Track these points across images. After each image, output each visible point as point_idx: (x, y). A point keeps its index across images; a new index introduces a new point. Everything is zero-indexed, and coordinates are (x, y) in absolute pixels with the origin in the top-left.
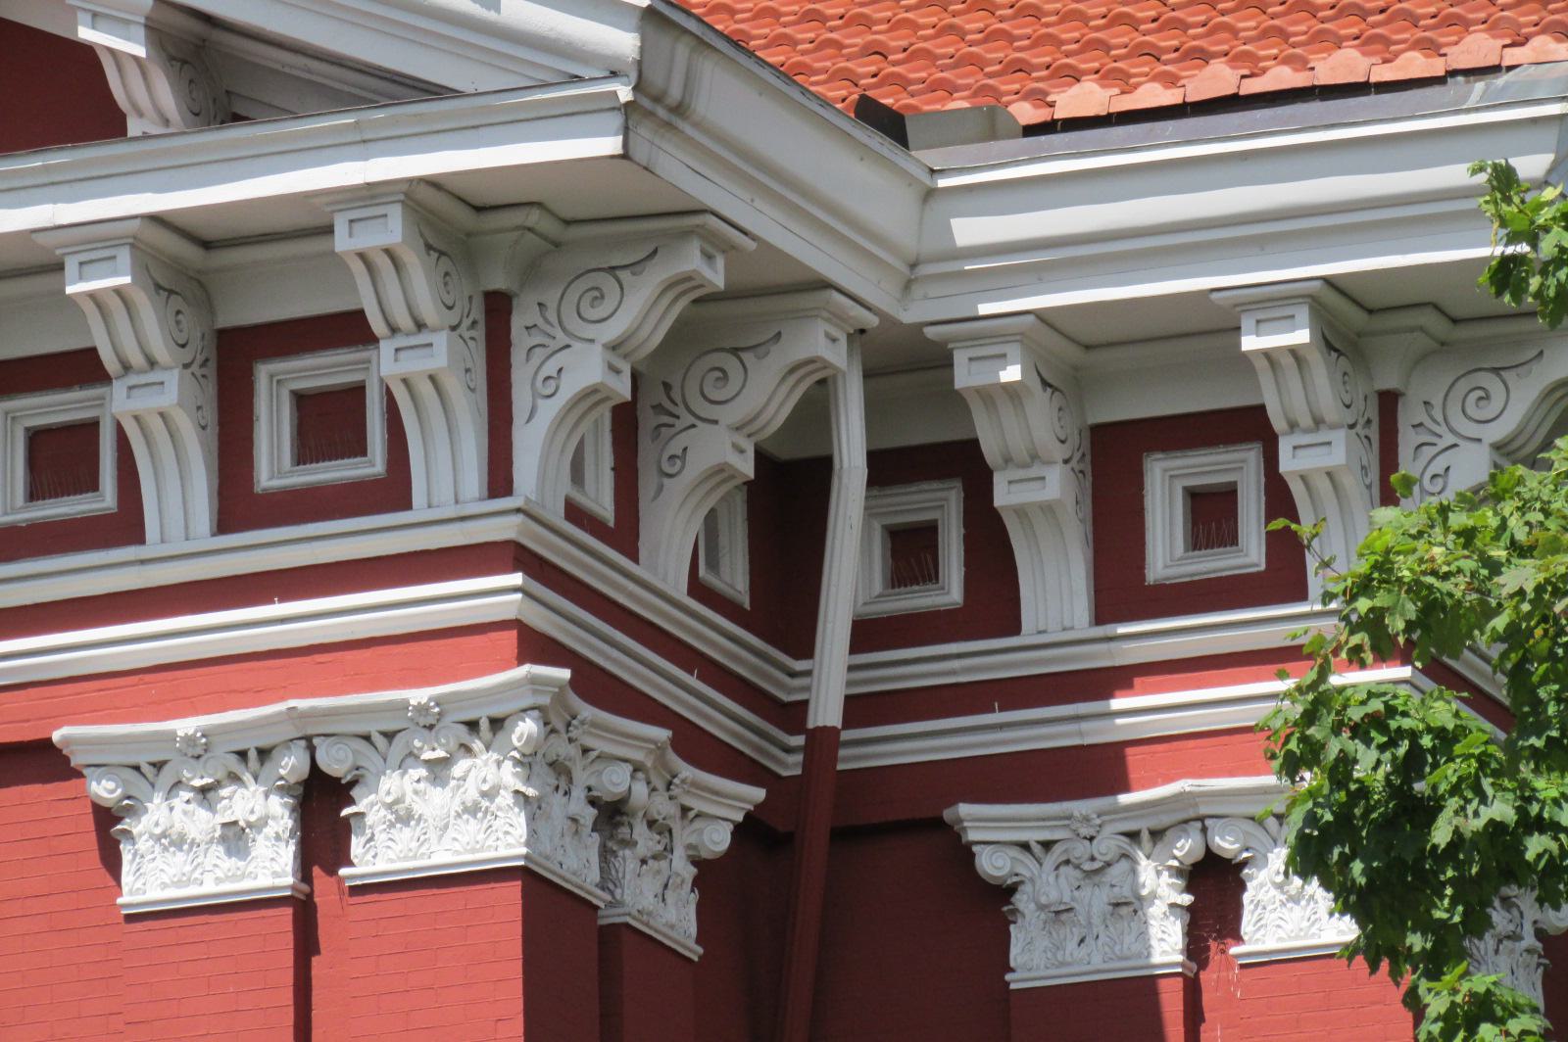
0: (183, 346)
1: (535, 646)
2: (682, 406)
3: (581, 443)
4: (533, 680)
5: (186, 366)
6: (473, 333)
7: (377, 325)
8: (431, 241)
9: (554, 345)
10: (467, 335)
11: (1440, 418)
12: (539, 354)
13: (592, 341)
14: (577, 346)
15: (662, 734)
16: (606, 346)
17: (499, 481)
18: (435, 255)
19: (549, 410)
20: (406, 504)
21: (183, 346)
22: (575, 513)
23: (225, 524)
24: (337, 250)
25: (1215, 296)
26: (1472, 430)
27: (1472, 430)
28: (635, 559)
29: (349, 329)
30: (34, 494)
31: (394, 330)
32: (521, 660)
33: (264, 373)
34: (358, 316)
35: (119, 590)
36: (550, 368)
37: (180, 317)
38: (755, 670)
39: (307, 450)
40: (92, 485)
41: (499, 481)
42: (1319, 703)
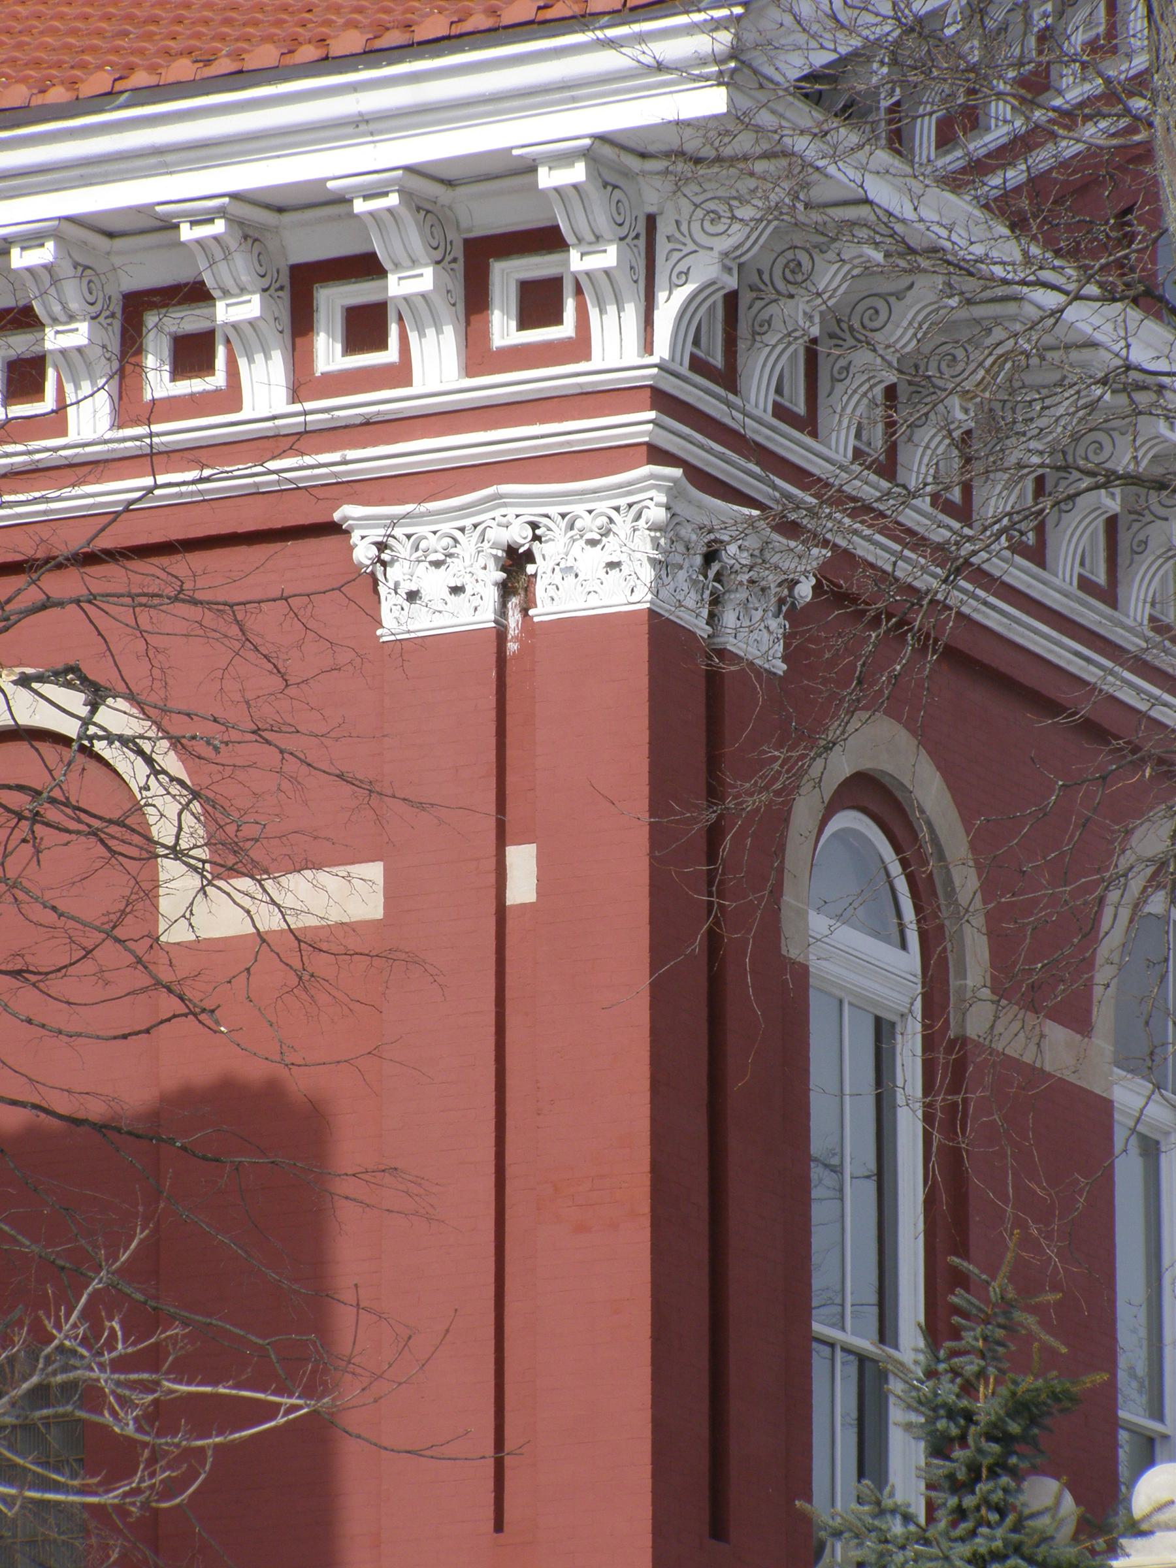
0: (620, 225)
1: (657, 454)
2: (770, 287)
5: (265, 290)
6: (280, 293)
8: (609, 179)
9: (686, 250)
10: (104, 323)
14: (702, 252)
16: (721, 253)
19: (682, 294)
20: (408, 382)
21: (263, 276)
23: (296, 394)
28: (735, 393)
29: (548, 239)
30: (523, 325)
31: (580, 241)
32: (649, 463)
33: (151, 319)
34: (556, 229)
37: (92, 284)
39: (526, 321)
40: (558, 320)
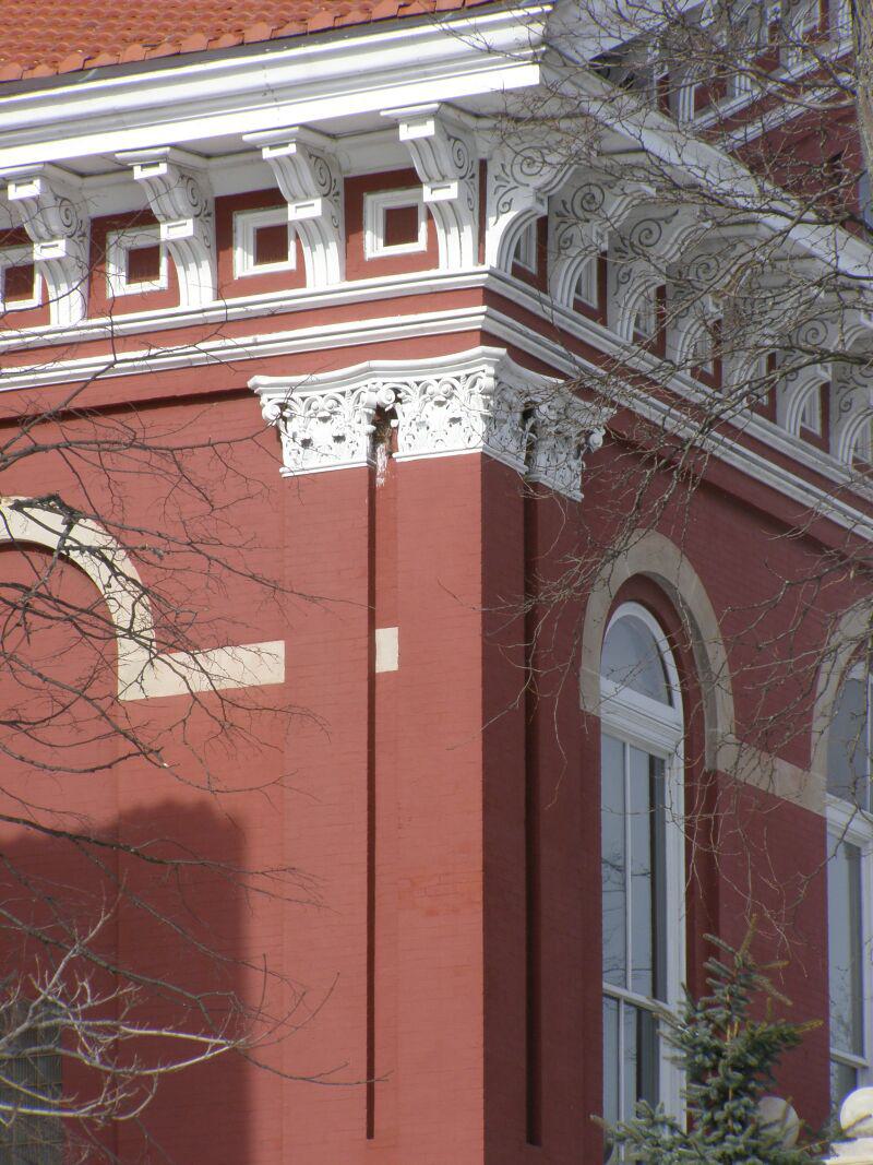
1: (488, 338)
3: (519, 240)
4: (484, 354)
7: (422, 177)
11: (509, 173)
12: (502, 191)
13: (528, 185)
15: (502, 351)
17: (481, 258)
18: (452, 141)
19: (506, 219)
22: (518, 272)
24: (264, 157)
25: (117, 155)
26: (523, 179)
27: (523, 179)
34: (412, 171)
35: (378, 657)
36: (506, 199)
38: (742, 463)
41: (481, 258)
42: (54, 62)
